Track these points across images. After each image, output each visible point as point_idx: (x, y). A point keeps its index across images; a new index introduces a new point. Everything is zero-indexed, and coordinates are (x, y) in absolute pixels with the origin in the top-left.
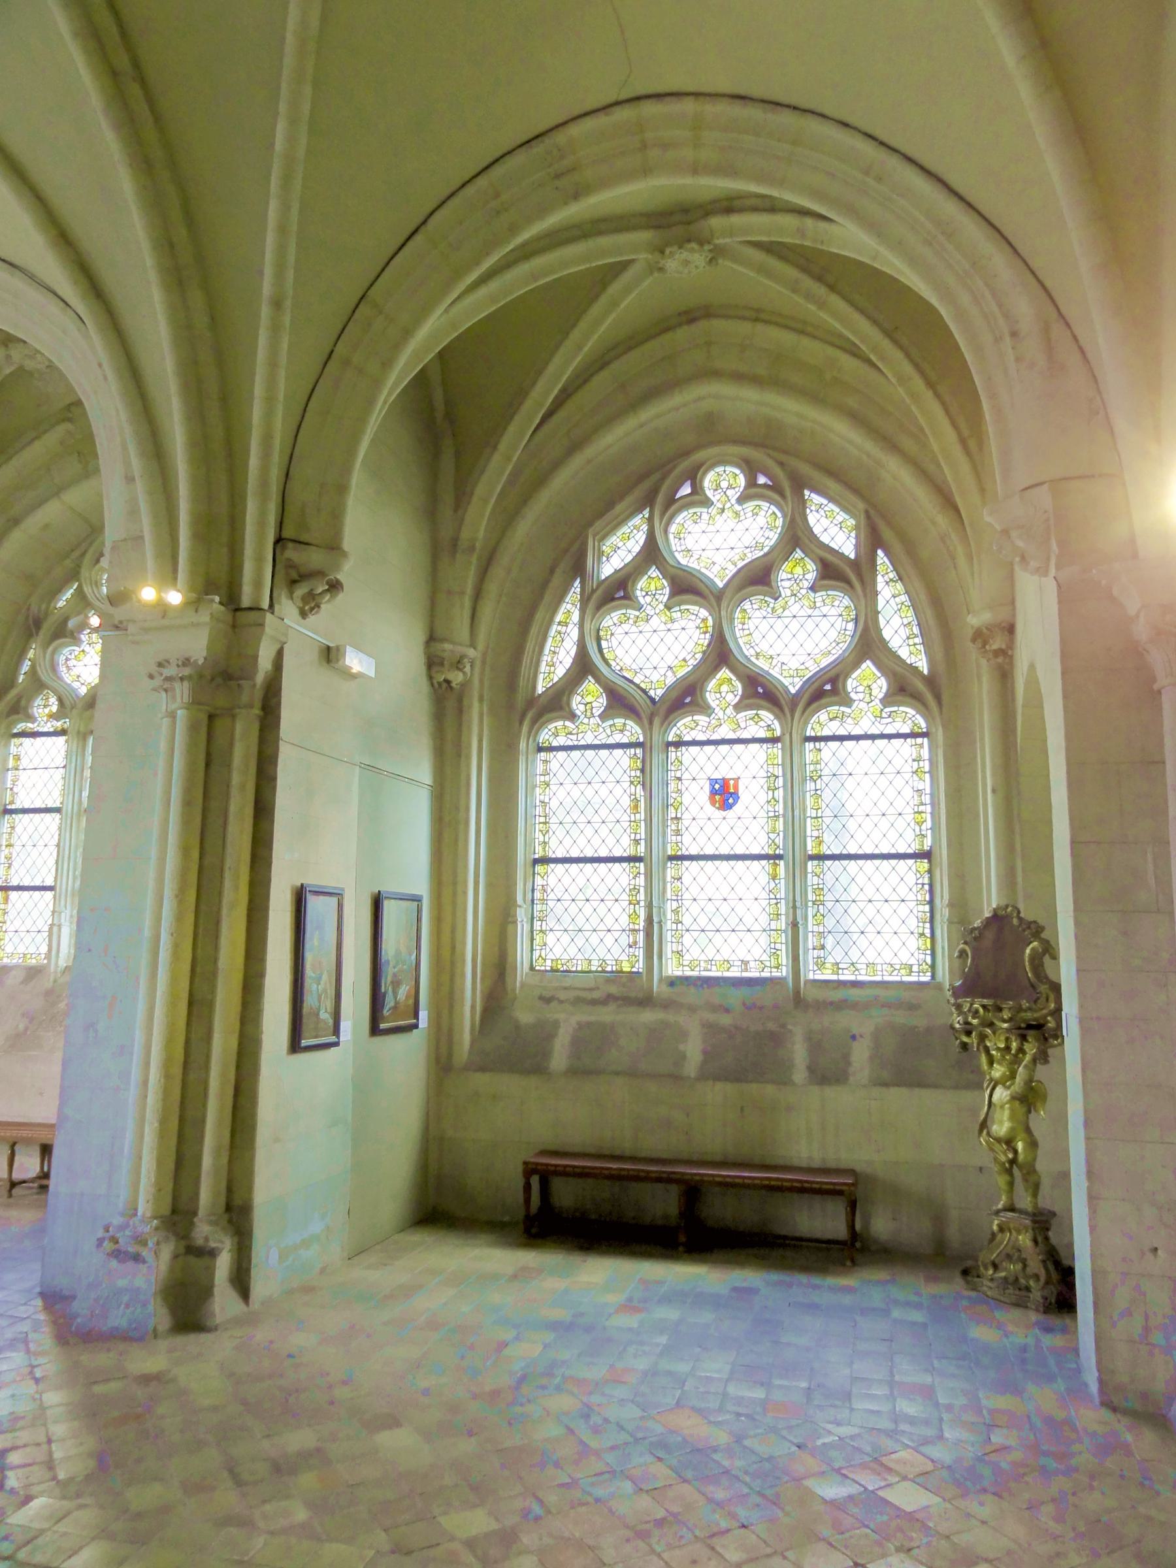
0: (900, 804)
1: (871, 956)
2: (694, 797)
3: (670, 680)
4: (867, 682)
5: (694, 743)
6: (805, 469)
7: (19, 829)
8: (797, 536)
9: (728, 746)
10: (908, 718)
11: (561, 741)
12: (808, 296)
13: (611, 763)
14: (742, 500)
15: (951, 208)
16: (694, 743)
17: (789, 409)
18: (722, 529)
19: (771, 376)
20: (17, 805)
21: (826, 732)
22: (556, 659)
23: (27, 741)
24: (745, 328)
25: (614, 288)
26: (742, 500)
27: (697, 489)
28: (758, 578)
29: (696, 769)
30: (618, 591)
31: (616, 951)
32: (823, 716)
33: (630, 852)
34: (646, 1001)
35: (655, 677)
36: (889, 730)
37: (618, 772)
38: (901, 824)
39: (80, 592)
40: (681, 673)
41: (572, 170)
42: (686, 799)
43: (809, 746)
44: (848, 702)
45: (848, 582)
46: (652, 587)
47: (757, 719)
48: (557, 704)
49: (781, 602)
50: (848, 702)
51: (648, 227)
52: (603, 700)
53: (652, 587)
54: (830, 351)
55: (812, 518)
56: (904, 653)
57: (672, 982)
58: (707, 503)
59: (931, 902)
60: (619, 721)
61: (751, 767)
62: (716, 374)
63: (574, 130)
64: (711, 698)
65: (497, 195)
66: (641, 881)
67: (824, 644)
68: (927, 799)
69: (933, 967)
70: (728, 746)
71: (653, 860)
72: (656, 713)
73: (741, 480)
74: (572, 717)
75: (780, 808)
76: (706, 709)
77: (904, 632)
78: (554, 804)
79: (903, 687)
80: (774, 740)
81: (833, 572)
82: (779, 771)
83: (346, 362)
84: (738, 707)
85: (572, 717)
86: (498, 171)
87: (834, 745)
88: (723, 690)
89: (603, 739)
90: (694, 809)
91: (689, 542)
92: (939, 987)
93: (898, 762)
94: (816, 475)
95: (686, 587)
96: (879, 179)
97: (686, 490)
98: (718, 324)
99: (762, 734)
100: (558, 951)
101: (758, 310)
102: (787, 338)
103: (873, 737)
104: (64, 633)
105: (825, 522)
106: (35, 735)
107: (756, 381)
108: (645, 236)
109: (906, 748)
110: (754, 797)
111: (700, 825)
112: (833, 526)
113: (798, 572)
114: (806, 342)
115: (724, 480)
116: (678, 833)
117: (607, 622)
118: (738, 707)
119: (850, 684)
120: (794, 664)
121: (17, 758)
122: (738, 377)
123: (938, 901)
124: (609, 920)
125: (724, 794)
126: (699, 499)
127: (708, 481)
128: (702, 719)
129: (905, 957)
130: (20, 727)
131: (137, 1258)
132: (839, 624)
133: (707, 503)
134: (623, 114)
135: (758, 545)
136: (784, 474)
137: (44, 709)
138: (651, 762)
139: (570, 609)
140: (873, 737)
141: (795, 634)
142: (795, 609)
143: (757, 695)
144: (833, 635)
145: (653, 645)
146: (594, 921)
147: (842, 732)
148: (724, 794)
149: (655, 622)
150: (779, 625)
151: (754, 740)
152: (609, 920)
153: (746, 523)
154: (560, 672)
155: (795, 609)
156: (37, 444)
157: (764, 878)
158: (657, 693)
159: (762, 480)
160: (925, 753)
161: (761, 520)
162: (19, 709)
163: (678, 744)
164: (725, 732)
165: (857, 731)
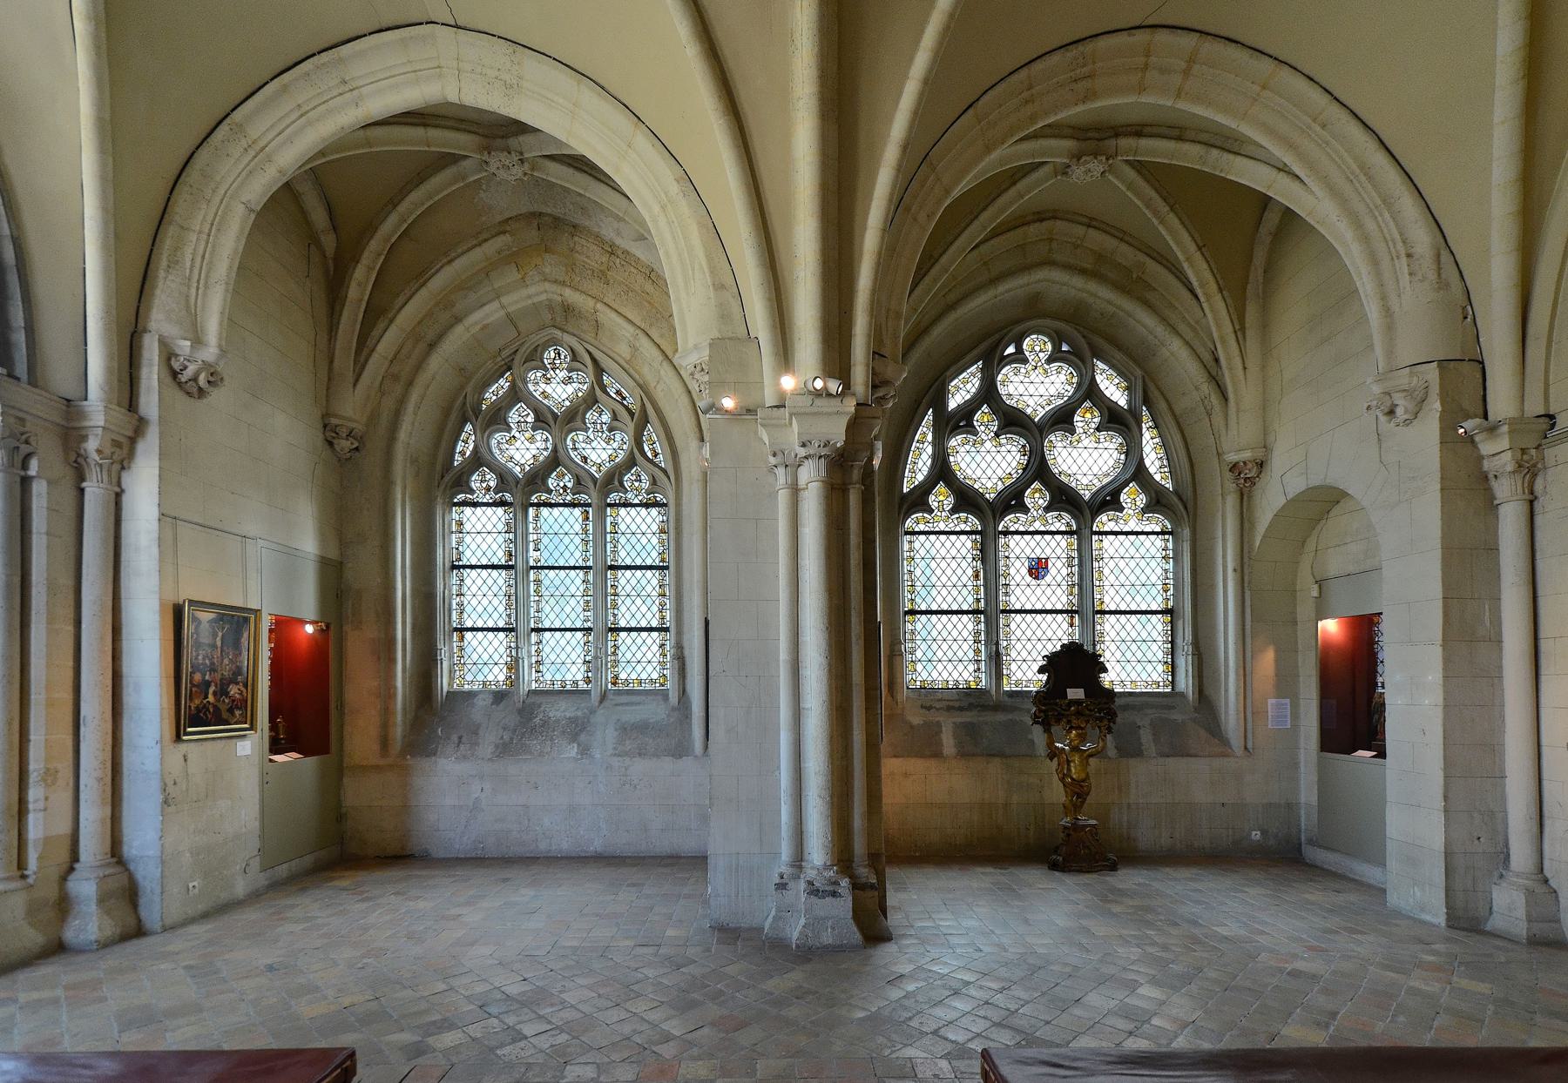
0: (1154, 578)
1: (1134, 676)
2: (1017, 572)
3: (1000, 487)
4: (1132, 497)
5: (1017, 532)
6: (1100, 342)
7: (468, 582)
8: (1089, 392)
9: (1035, 539)
10: (1155, 523)
11: (922, 527)
12: (1156, 213)
13: (958, 545)
14: (1050, 361)
15: (1379, 159)
16: (1017, 532)
17: (1101, 296)
18: (1036, 384)
19: (1097, 269)
20: (464, 562)
21: (1106, 529)
22: (919, 465)
23: (468, 510)
24: (1080, 230)
25: (1020, 186)
26: (1050, 361)
27: (1019, 350)
28: (1062, 419)
29: (1018, 550)
30: (961, 421)
31: (966, 675)
32: (1104, 517)
33: (974, 607)
34: (998, 707)
35: (989, 485)
36: (1148, 529)
37: (964, 551)
38: (1154, 592)
39: (513, 386)
40: (1008, 482)
41: (1090, 76)
42: (1012, 571)
43: (1095, 538)
44: (1121, 509)
45: (1127, 426)
46: (984, 418)
47: (1060, 518)
48: (919, 501)
49: (1076, 437)
50: (1121, 509)
51: (1072, 137)
52: (951, 499)
53: (984, 418)
54: (1142, 257)
55: (1098, 378)
56: (1157, 477)
57: (1012, 694)
58: (1025, 361)
59: (1172, 642)
60: (963, 515)
61: (1057, 549)
62: (1050, 263)
63: (1102, 43)
64: (1027, 501)
65: (1030, 87)
66: (982, 626)
67: (1105, 469)
68: (1171, 575)
69: (1173, 682)
70: (1035, 539)
71: (991, 613)
72: (989, 513)
73: (1049, 346)
74: (931, 511)
75: (1076, 579)
76: (1026, 510)
77: (1157, 463)
78: (918, 572)
79: (1157, 501)
80: (1070, 533)
81: (1115, 420)
82: (1075, 554)
83: (908, 209)
84: (1047, 509)
85: (931, 511)
86: (1038, 66)
87: (1111, 537)
88: (1036, 497)
89: (951, 527)
90: (1018, 578)
91: (1011, 389)
92: (1182, 695)
93: (1153, 551)
94: (1106, 346)
95: (1012, 421)
96: (1323, 126)
97: (1011, 350)
98: (1059, 225)
99: (1063, 528)
100: (925, 675)
101: (1091, 219)
102: (1110, 243)
103: (1137, 533)
104: (496, 419)
105: (1107, 383)
106: (475, 505)
107: (1083, 272)
108: (1068, 144)
109: (1158, 542)
110: (1058, 571)
111: (1021, 591)
112: (1113, 389)
113: (1086, 419)
114: (1124, 247)
115: (1036, 345)
116: (1006, 594)
117: (953, 442)
118: (1047, 509)
119: (1123, 497)
120: (1085, 481)
121: (460, 523)
122: (1067, 267)
123: (1179, 641)
124: (960, 654)
125: (1038, 569)
126: (1020, 358)
127: (1026, 344)
128: (1022, 517)
129: (1155, 677)
130: (461, 497)
131: (834, 894)
132: (1116, 455)
133: (1025, 361)
134: (1141, 37)
135: (1060, 396)
136: (1080, 343)
137: (483, 482)
138: (1083, 533)
139: (926, 429)
140: (1137, 533)
141: (1086, 459)
142: (1086, 442)
143: (1061, 501)
144: (1111, 462)
145: (988, 462)
146: (950, 654)
147: (1117, 529)
148: (1038, 569)
149: (988, 445)
150: (1075, 453)
151: (1058, 533)
152: (960, 654)
153: (1053, 378)
154: (920, 477)
155: (1086, 442)
156: (478, 250)
157: (1065, 626)
158: (991, 496)
159: (1065, 348)
160: (1170, 545)
161: (1062, 377)
162: (460, 482)
163: (1006, 533)
164: (1037, 526)
165: (1126, 529)
